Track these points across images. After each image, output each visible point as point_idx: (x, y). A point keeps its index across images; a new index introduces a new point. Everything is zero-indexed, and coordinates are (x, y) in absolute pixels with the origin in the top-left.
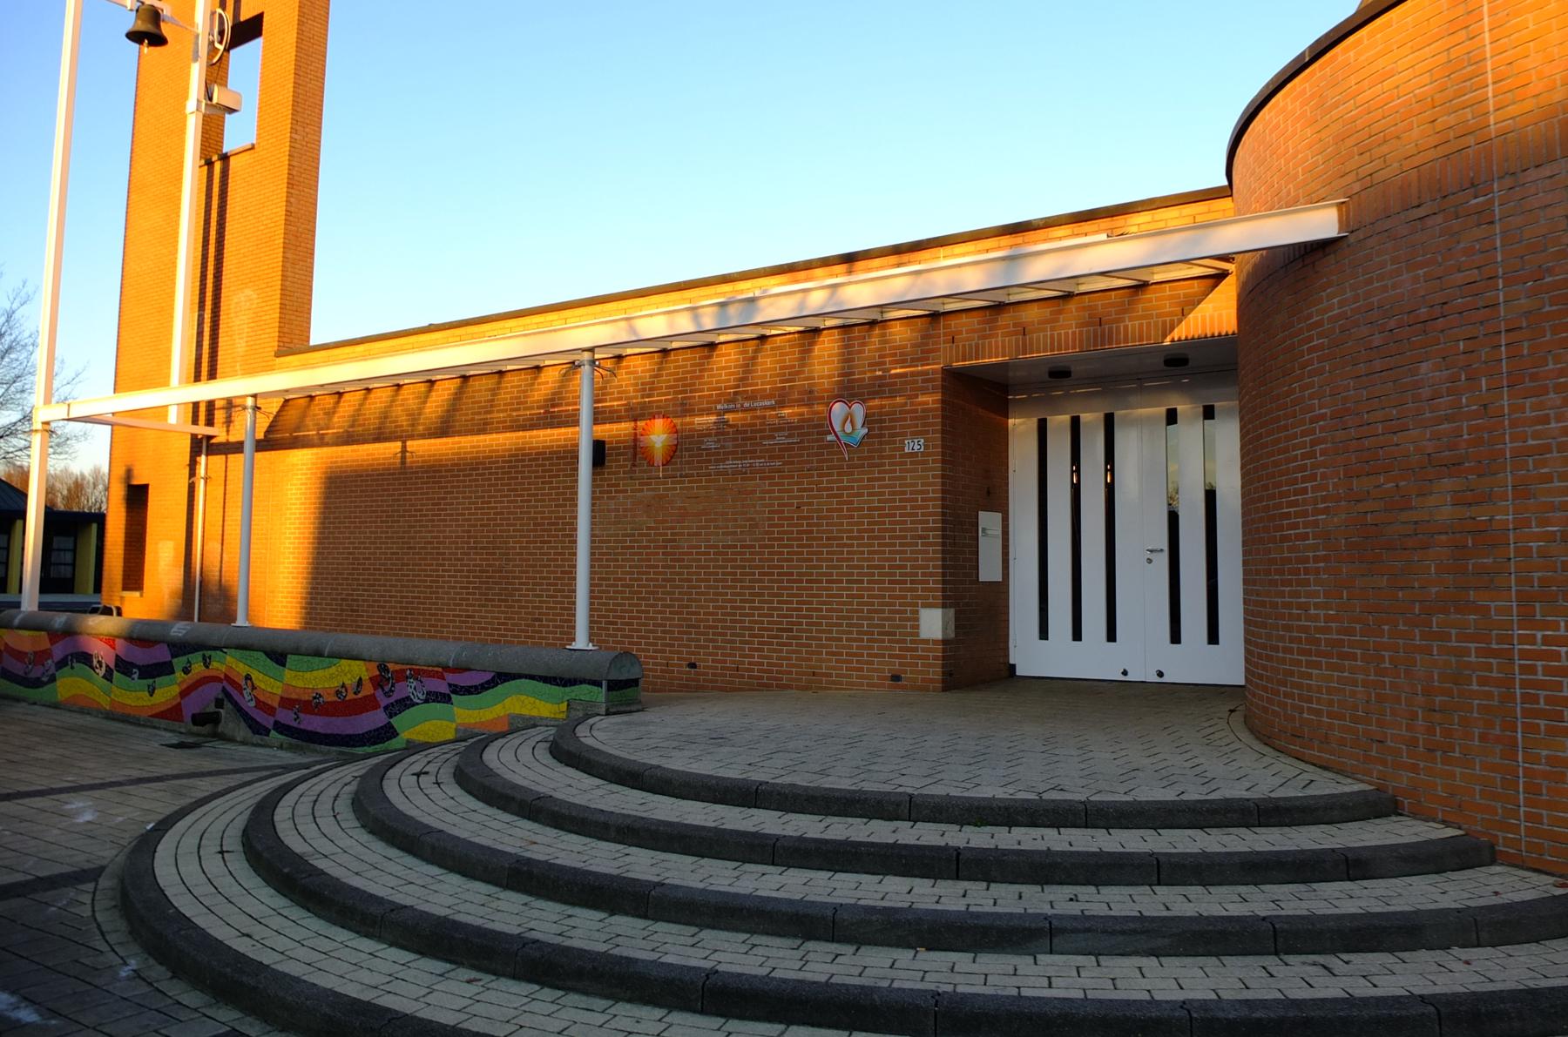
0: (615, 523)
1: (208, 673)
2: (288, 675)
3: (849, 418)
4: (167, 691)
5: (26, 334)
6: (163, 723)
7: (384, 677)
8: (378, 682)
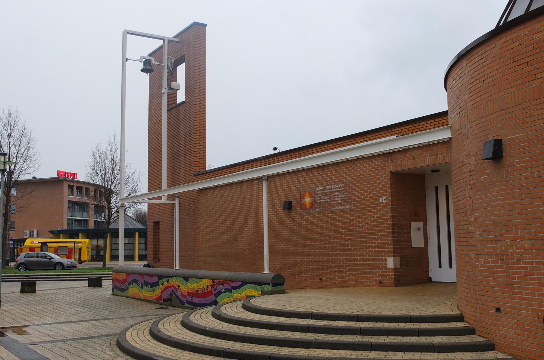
1: (168, 285)
2: (189, 284)
4: (158, 291)
7: (216, 283)
8: (212, 286)
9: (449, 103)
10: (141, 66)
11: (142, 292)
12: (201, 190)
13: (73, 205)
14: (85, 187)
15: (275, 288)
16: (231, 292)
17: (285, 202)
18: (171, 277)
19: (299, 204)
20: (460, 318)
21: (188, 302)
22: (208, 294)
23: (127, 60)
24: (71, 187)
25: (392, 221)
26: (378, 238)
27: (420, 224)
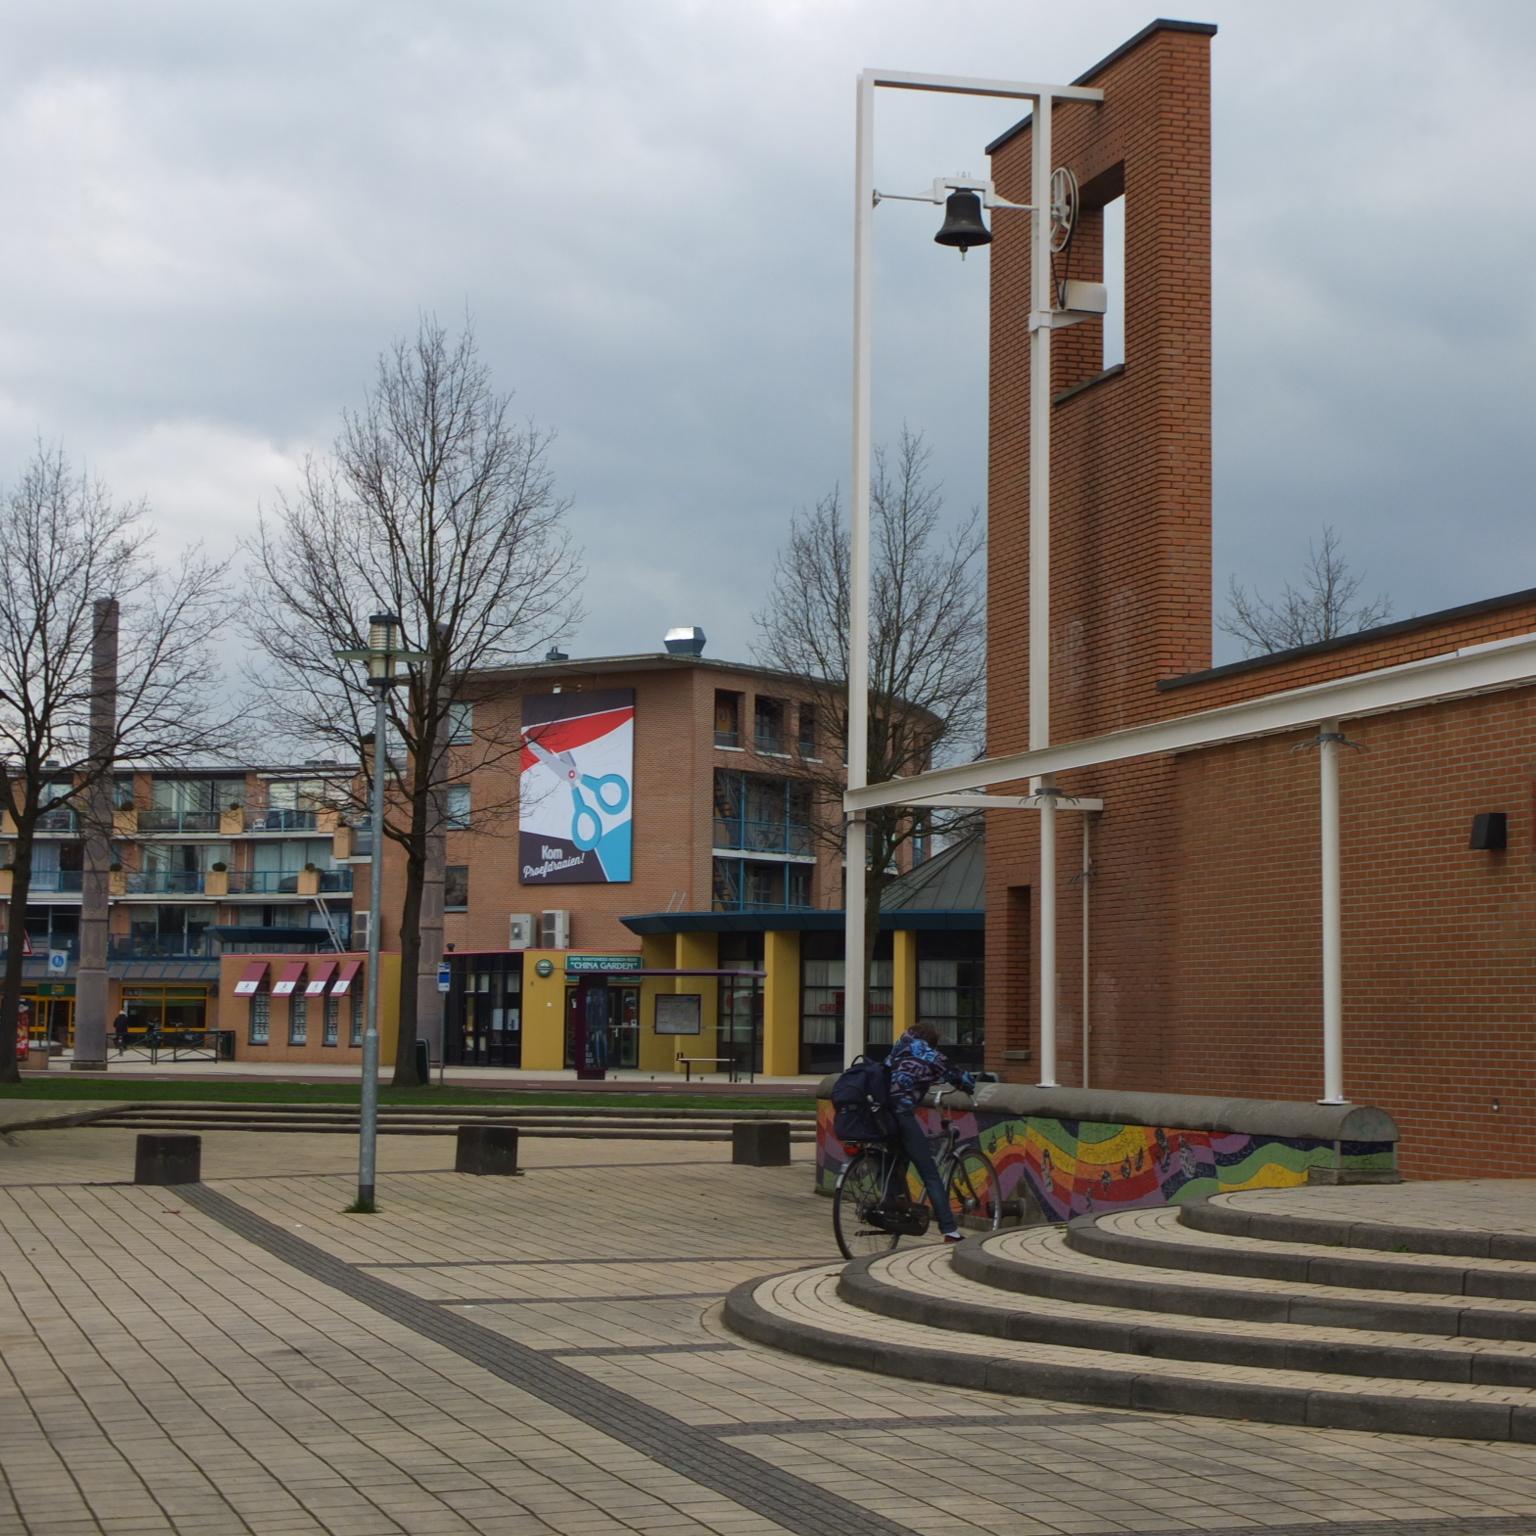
2: (1081, 1147)
8: (1157, 1152)
12: (1183, 756)
14: (795, 696)
15: (1354, 1161)
16: (1027, 1153)
17: (1478, 819)
18: (1014, 1116)
24: (727, 702)
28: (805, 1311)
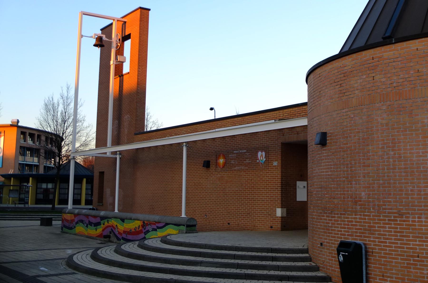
0: (212, 184)
1: (108, 225)
2: (125, 224)
3: (262, 155)
4: (100, 230)
5: (81, 117)
6: (97, 238)
7: (144, 225)
8: (143, 226)
9: (309, 99)
10: (94, 41)
11: (87, 231)
13: (24, 151)
14: (36, 133)
18: (110, 218)
19: (215, 164)
20: (306, 251)
21: (124, 239)
22: (140, 232)
23: (82, 36)
25: (281, 180)
26: (271, 193)
27: (305, 183)
28: (83, 262)
